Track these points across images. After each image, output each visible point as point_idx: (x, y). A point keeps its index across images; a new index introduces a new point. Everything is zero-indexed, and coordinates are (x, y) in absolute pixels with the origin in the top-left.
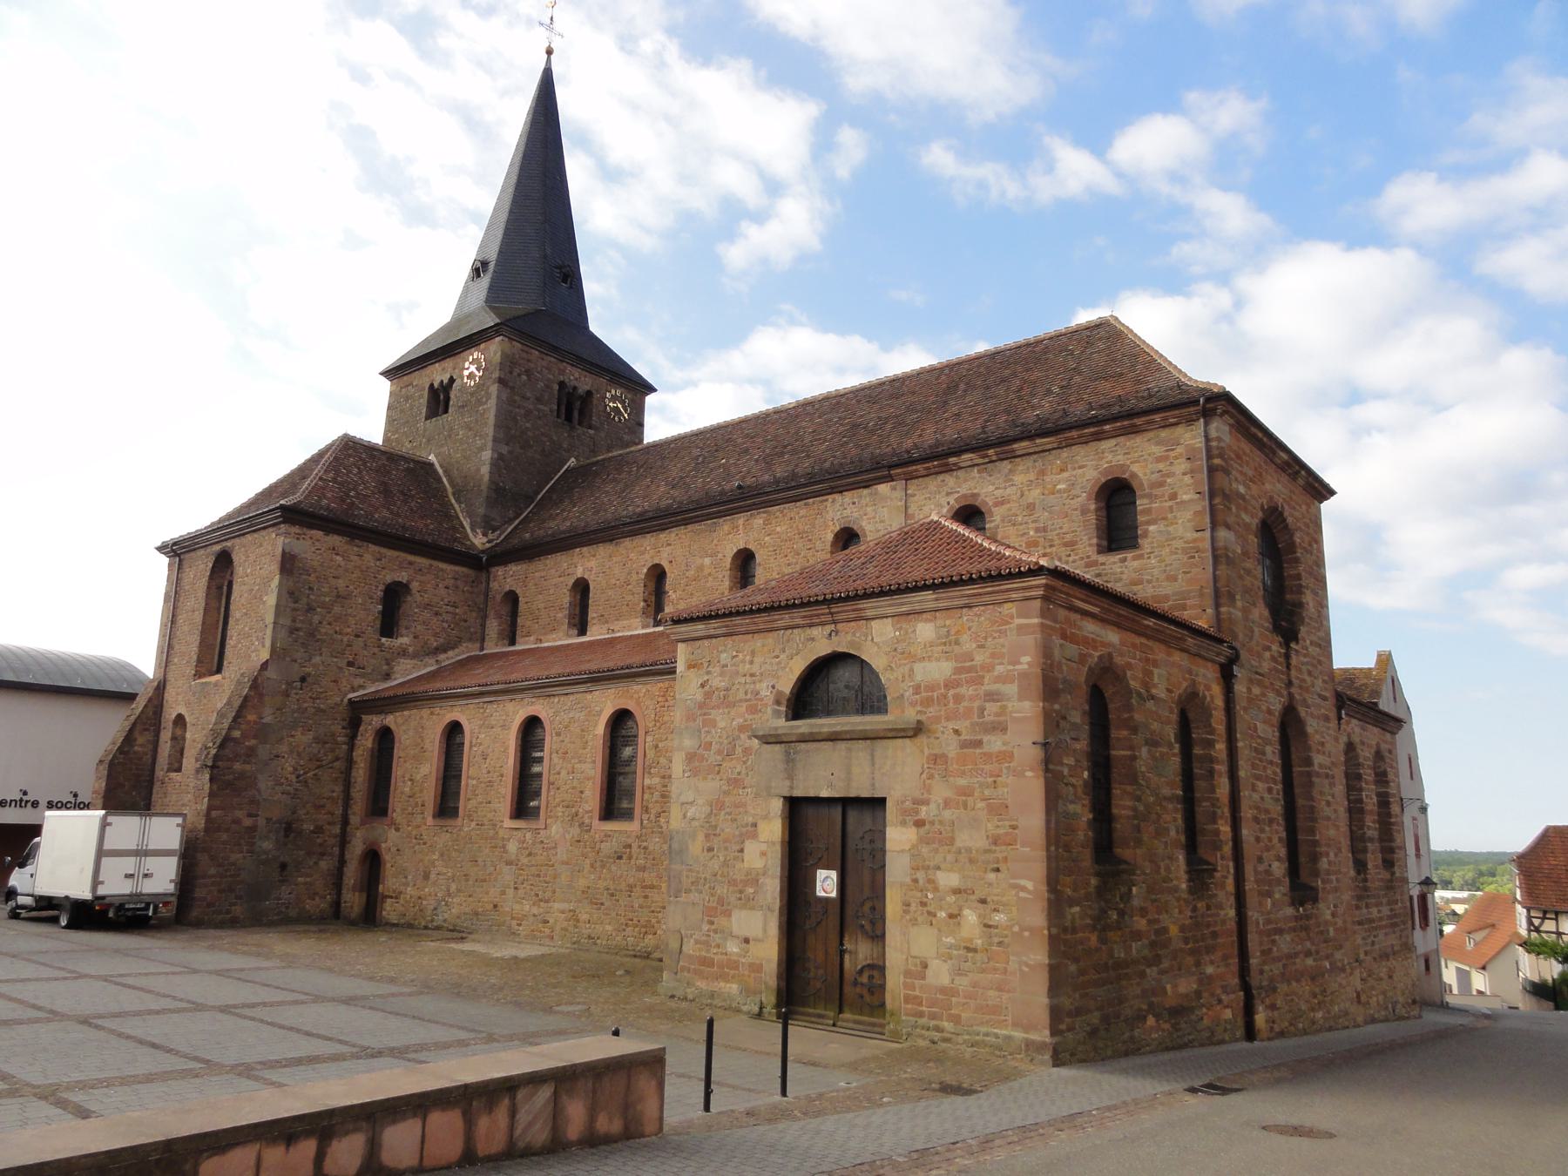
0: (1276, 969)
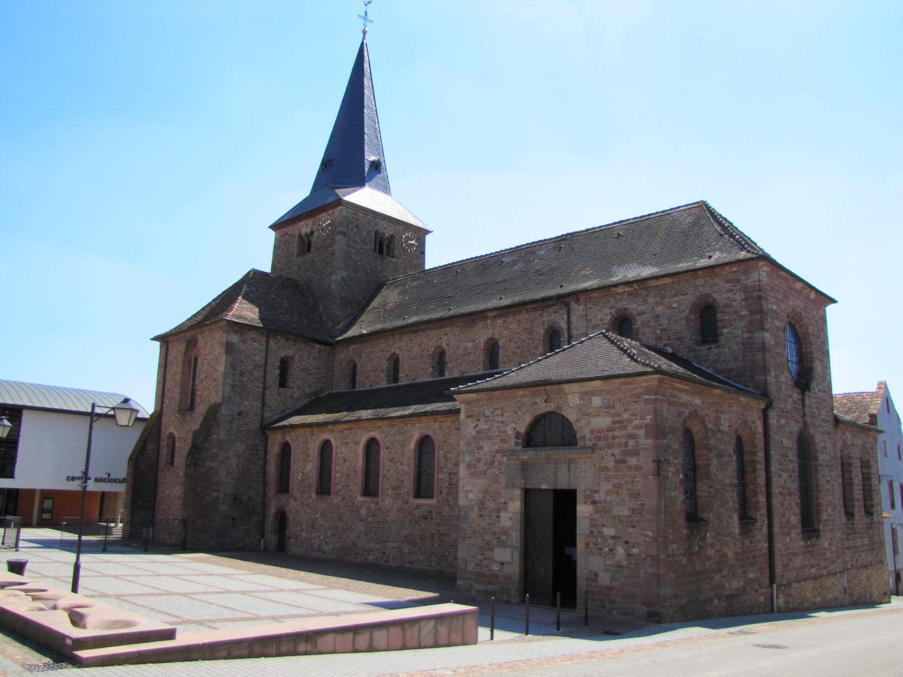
0: (792, 575)
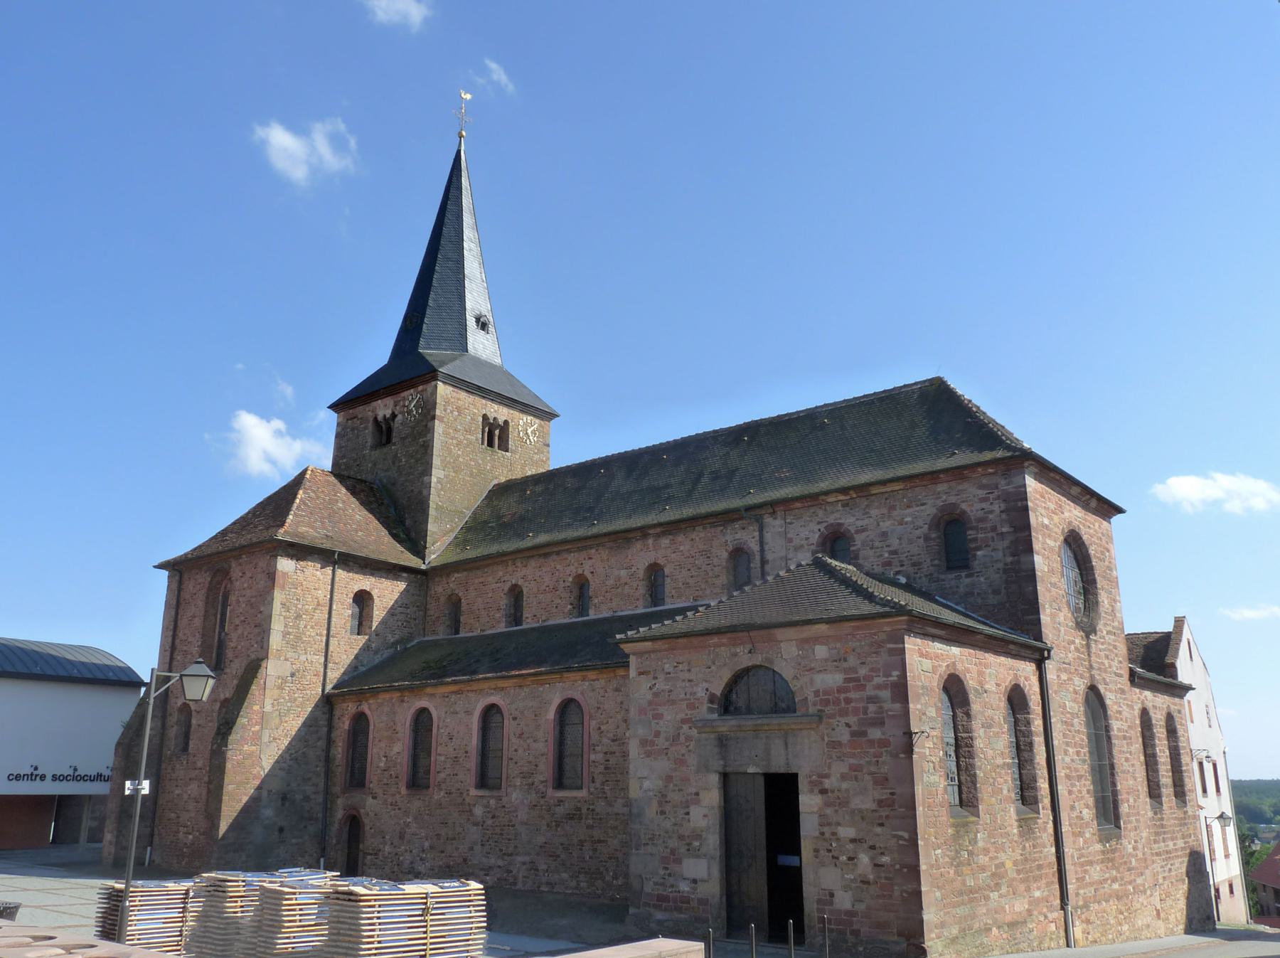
0: (1089, 892)
